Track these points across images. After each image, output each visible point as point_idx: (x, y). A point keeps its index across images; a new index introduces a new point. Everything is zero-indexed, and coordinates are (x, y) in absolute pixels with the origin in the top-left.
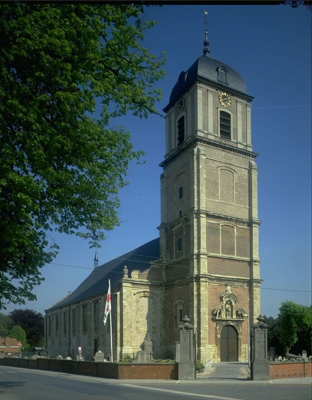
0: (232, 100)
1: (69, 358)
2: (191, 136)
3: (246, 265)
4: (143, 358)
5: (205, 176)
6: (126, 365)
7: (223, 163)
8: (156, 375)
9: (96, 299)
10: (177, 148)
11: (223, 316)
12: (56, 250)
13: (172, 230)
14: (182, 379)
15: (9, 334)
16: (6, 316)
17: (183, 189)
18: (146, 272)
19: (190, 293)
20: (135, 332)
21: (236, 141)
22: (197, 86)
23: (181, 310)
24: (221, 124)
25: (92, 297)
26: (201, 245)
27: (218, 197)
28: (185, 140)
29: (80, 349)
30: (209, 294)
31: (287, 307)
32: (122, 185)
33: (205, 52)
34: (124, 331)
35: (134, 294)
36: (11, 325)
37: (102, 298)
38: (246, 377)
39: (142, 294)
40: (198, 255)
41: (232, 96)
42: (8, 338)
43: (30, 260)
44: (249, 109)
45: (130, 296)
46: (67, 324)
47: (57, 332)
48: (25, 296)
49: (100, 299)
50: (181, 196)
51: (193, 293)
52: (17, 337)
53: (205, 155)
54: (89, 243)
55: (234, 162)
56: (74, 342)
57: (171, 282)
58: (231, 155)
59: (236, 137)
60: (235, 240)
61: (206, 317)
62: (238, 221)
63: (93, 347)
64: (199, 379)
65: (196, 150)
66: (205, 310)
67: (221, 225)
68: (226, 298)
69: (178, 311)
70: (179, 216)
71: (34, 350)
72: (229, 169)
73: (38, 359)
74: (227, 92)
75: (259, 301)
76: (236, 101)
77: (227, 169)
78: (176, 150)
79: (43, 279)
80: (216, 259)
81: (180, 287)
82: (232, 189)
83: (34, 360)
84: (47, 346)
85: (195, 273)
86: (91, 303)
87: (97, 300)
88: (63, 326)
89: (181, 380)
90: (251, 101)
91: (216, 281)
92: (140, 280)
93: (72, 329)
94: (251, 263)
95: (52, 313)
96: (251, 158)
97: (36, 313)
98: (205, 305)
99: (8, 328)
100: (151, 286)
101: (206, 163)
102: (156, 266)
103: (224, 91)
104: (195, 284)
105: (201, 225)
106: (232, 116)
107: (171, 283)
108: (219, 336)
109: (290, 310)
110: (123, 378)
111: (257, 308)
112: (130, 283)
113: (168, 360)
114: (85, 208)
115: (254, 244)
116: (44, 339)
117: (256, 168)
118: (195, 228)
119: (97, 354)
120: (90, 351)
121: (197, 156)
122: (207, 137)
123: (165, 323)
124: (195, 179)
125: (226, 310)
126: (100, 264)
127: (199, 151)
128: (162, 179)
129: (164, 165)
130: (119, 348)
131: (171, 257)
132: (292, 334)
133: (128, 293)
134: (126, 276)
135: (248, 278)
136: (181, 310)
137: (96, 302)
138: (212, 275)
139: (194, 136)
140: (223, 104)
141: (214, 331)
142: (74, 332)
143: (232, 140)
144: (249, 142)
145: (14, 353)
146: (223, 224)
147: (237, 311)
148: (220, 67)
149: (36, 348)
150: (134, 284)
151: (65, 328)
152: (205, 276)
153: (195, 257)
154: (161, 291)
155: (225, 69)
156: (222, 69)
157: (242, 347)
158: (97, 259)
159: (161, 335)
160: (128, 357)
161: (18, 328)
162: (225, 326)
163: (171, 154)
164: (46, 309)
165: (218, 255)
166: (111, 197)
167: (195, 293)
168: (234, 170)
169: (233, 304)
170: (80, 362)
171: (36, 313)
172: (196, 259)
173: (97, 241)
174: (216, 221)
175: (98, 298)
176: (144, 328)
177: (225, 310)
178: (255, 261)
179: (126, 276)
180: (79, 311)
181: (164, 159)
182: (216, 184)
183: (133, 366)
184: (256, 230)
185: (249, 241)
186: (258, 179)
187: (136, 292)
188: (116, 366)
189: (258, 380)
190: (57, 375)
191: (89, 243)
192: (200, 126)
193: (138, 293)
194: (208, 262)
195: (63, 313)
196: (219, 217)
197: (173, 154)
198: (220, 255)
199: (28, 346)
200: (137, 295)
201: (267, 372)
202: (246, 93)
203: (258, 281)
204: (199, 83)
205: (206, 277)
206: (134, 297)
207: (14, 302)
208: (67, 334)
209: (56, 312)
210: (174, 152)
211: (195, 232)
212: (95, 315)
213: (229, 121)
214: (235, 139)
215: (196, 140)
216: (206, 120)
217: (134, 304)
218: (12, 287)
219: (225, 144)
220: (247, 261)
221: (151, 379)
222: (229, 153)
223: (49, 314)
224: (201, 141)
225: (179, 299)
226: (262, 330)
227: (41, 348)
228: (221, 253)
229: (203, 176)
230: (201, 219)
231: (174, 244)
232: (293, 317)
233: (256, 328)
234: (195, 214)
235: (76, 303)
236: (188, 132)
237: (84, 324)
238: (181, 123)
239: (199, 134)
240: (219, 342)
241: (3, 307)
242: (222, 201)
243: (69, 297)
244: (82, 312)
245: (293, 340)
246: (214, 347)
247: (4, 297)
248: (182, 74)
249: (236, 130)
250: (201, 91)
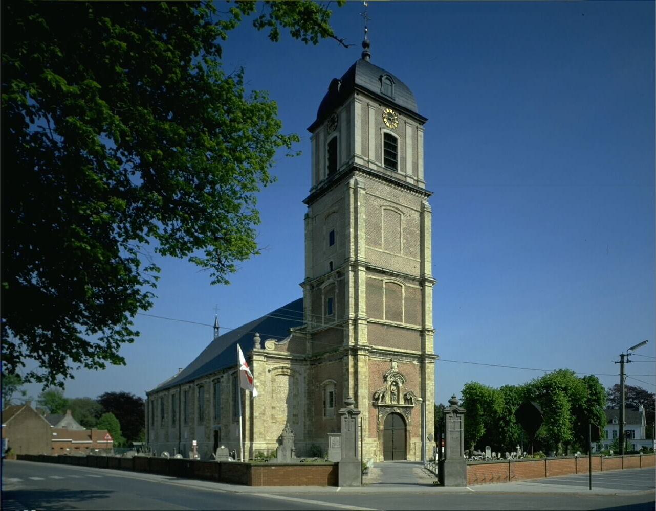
0: (399, 119)
1: (179, 457)
2: (346, 164)
3: (417, 335)
4: (284, 456)
5: (364, 217)
6: (263, 466)
7: (388, 201)
8: (306, 480)
9: (216, 377)
10: (327, 179)
11: (388, 401)
12: (155, 273)
13: (321, 287)
14: (345, 485)
15: (97, 424)
16: (94, 401)
17: (335, 233)
18: (286, 342)
19: (344, 371)
20: (270, 421)
21: (404, 174)
22: (354, 98)
23: (331, 393)
24: (385, 151)
25: (211, 374)
26: (359, 306)
27: (380, 245)
28: (337, 169)
29: (195, 443)
30: (370, 373)
31: (473, 389)
32: (265, 181)
33: (365, 55)
34: (254, 420)
35: (269, 371)
36: (100, 413)
37: (224, 375)
38: (431, 482)
39: (280, 370)
40: (355, 321)
41: (400, 114)
42: (94, 429)
43: (117, 300)
44: (421, 133)
45: (263, 374)
46: (177, 410)
47: (162, 421)
48: (105, 358)
49: (222, 377)
50: (332, 242)
51: (348, 370)
52: (109, 428)
53: (364, 189)
54: (211, 276)
55: (402, 202)
56: (186, 434)
57: (319, 355)
58: (398, 191)
59: (404, 168)
60: (403, 302)
61: (365, 403)
62: (406, 277)
63: (212, 442)
64: (367, 485)
65: (352, 182)
66: (364, 393)
67: (384, 281)
68: (391, 378)
69: (328, 394)
70: (329, 269)
71: (132, 446)
72: (395, 210)
73: (134, 458)
74: (394, 109)
75: (433, 382)
76: (405, 122)
77: (393, 209)
78: (326, 182)
79: (137, 334)
80: (380, 327)
81: (331, 363)
82: (399, 235)
83: (128, 459)
84: (148, 440)
85: (350, 344)
86: (210, 382)
87: (219, 378)
88: (170, 414)
89: (343, 486)
90: (424, 123)
91: (378, 355)
92: (276, 352)
93: (182, 418)
94: (423, 332)
95: (156, 396)
96: (423, 196)
97: (134, 397)
98: (364, 386)
99: (96, 416)
100: (293, 360)
101: (366, 199)
102: (298, 335)
103: (389, 107)
104: (351, 358)
105: (360, 281)
106: (399, 141)
107: (319, 357)
108: (382, 427)
109: (476, 393)
110: (259, 485)
111: (430, 391)
112: (263, 355)
113: (315, 458)
114: (207, 227)
115: (426, 308)
116: (146, 431)
117: (430, 210)
118: (351, 284)
119: (219, 451)
120: (207, 446)
121: (354, 189)
122: (367, 165)
123: (309, 410)
124: (351, 220)
125: (392, 393)
126: (222, 332)
127: (356, 183)
128: (307, 220)
129: (310, 201)
130: (248, 443)
131: (319, 319)
132: (478, 424)
133: (261, 369)
134: (258, 346)
135: (420, 353)
136: (331, 393)
137: (216, 381)
138: (374, 347)
139: (350, 163)
140: (388, 124)
141: (375, 420)
142: (186, 422)
143: (399, 172)
144: (421, 176)
145: (103, 449)
146: (387, 281)
147: (405, 395)
148: (381, 75)
149: (135, 443)
150: (269, 357)
151: (174, 416)
152: (364, 348)
153: (351, 322)
154: (305, 367)
155: (390, 78)
156: (387, 78)
157: (411, 442)
158: (217, 326)
159: (305, 426)
160: (261, 455)
161: (110, 416)
162: (390, 414)
163: (319, 187)
164: (148, 391)
165: (381, 321)
166: (244, 210)
167: (351, 370)
168: (401, 212)
169: (400, 385)
170: (194, 462)
171: (134, 397)
172: (352, 325)
173: (223, 275)
174: (378, 276)
175: (219, 376)
176: (282, 415)
177: (390, 393)
178: (428, 331)
179: (258, 346)
180: (194, 393)
181: (309, 194)
182: (379, 229)
183: (273, 468)
184: (429, 290)
185: (421, 305)
186: (432, 225)
187: (271, 367)
188: (248, 467)
189: (451, 486)
190: (160, 480)
191: (211, 276)
192: (358, 150)
193: (274, 369)
194: (368, 329)
195: (171, 397)
196: (383, 272)
197: (322, 187)
198: (384, 321)
199: (123, 440)
200: (273, 372)
201: (464, 474)
202: (417, 111)
203: (432, 357)
204: (358, 94)
205: (365, 350)
206: (269, 375)
207: (87, 365)
208: (177, 422)
209: (161, 394)
210: (323, 184)
211: (352, 290)
212: (215, 398)
213: (395, 148)
214: (403, 171)
215: (352, 169)
216: (366, 145)
217: (269, 384)
218: (85, 344)
219: (391, 177)
220: (418, 331)
221: (300, 485)
222: (395, 188)
223: (152, 398)
224: (360, 170)
225: (330, 378)
226: (457, 417)
227: (140, 443)
228: (384, 318)
229: (362, 216)
230: (360, 272)
231: (323, 306)
232: (480, 402)
233: (448, 413)
234: (351, 265)
235: (189, 382)
236: (342, 158)
237: (200, 410)
238: (333, 146)
239: (357, 161)
240: (382, 434)
241: (68, 375)
242: (386, 252)
243: (179, 375)
244: (197, 394)
245: (478, 432)
246: (375, 441)
247: (69, 358)
248: (335, 82)
249: (404, 159)
250: (359, 105)
